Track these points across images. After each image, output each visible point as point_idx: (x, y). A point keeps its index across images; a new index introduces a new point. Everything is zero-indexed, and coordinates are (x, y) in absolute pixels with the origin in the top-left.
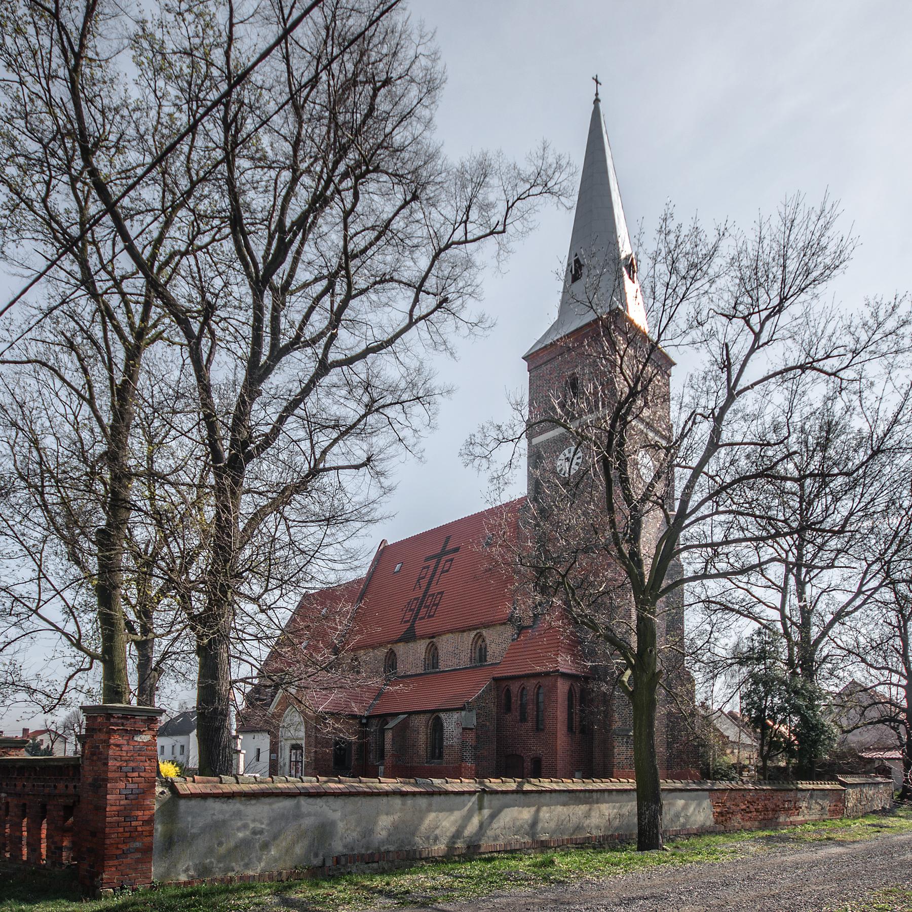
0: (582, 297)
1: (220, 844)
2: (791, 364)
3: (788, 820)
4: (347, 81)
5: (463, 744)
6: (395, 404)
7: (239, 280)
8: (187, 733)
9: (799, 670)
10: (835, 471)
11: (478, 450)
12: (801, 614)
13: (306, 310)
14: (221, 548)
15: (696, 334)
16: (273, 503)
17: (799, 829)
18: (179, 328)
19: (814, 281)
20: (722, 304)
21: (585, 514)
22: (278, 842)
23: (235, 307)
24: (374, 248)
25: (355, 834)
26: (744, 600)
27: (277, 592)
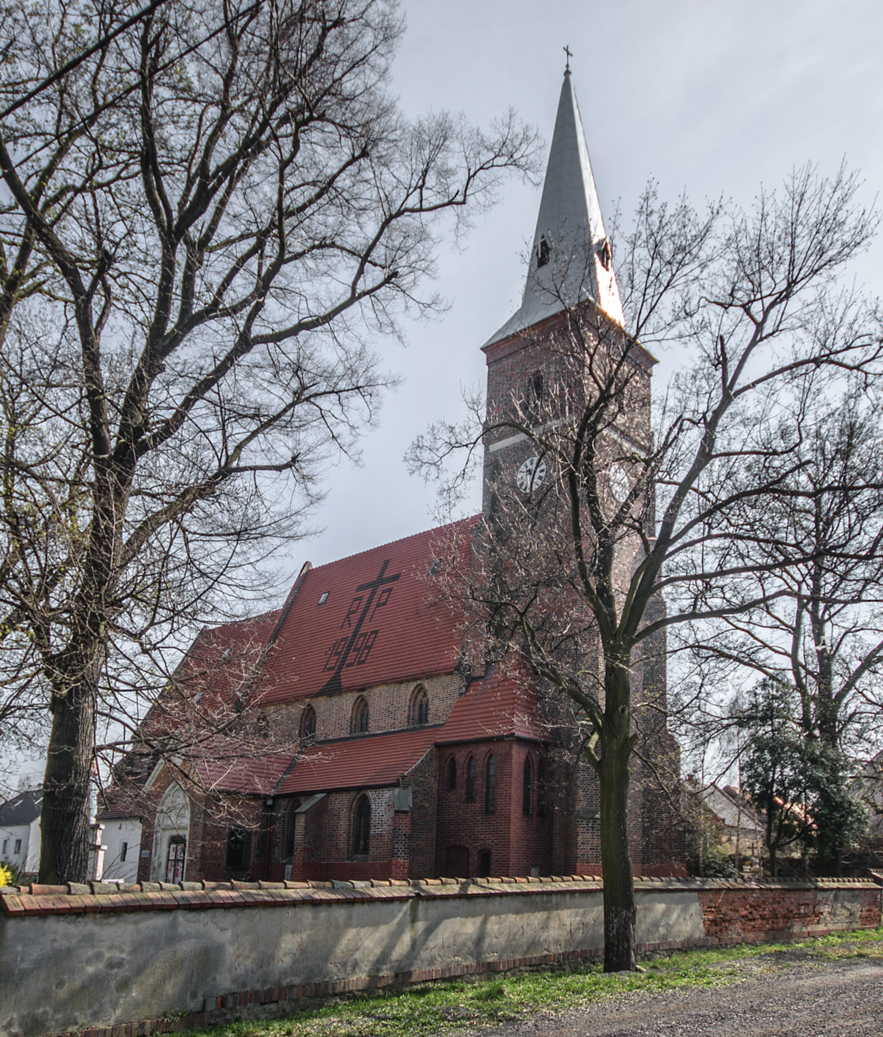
0: (549, 285)
1: (60, 984)
2: (802, 357)
3: (804, 930)
4: (292, 15)
5: (395, 831)
6: (330, 393)
7: (147, 228)
8: (25, 821)
9: (817, 732)
10: (861, 482)
11: (426, 455)
12: (819, 660)
13: (227, 272)
14: (96, 565)
15: (683, 326)
16: (169, 509)
17: (819, 943)
18: (64, 281)
19: (830, 261)
20: (716, 291)
21: (548, 538)
22: (141, 978)
23: (139, 261)
24: (314, 207)
25: (248, 963)
26: (744, 644)
27: (166, 626)
